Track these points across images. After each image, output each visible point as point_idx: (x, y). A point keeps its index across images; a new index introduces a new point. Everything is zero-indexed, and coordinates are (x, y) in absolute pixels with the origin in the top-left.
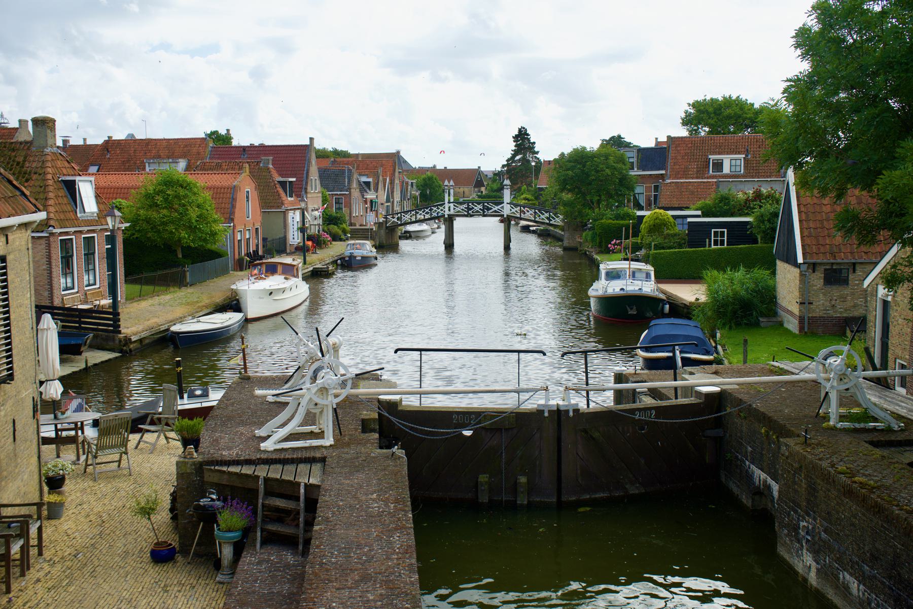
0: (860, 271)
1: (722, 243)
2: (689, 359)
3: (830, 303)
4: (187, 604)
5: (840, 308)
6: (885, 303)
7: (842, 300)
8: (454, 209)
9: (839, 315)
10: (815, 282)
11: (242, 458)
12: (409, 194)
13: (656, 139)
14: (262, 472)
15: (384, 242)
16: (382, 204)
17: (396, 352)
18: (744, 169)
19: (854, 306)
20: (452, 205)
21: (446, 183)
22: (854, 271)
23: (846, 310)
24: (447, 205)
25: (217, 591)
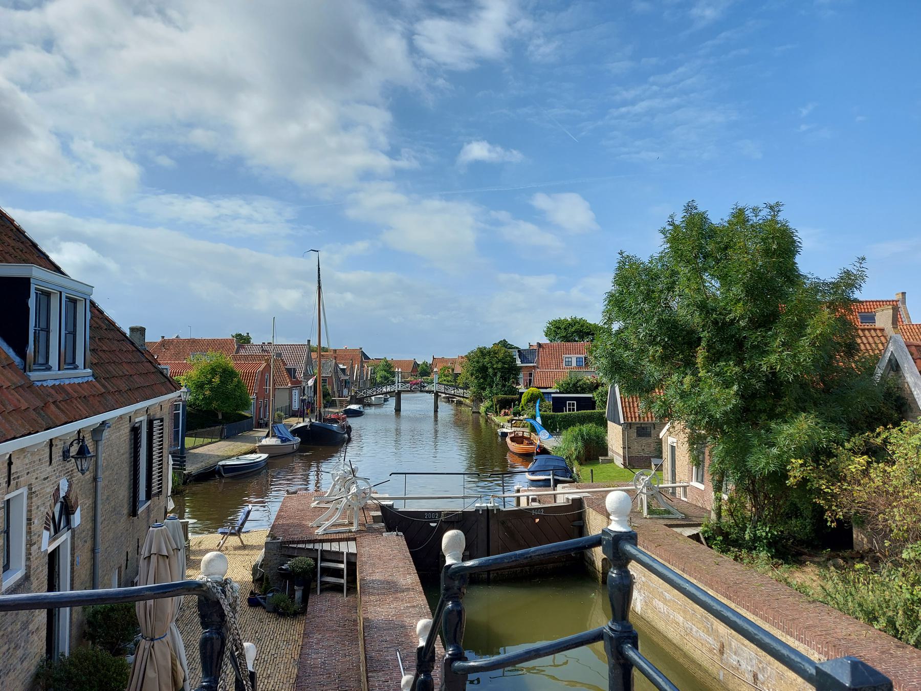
1: (573, 410)
2: (558, 480)
6: (673, 448)
17: (390, 475)
21: (396, 370)
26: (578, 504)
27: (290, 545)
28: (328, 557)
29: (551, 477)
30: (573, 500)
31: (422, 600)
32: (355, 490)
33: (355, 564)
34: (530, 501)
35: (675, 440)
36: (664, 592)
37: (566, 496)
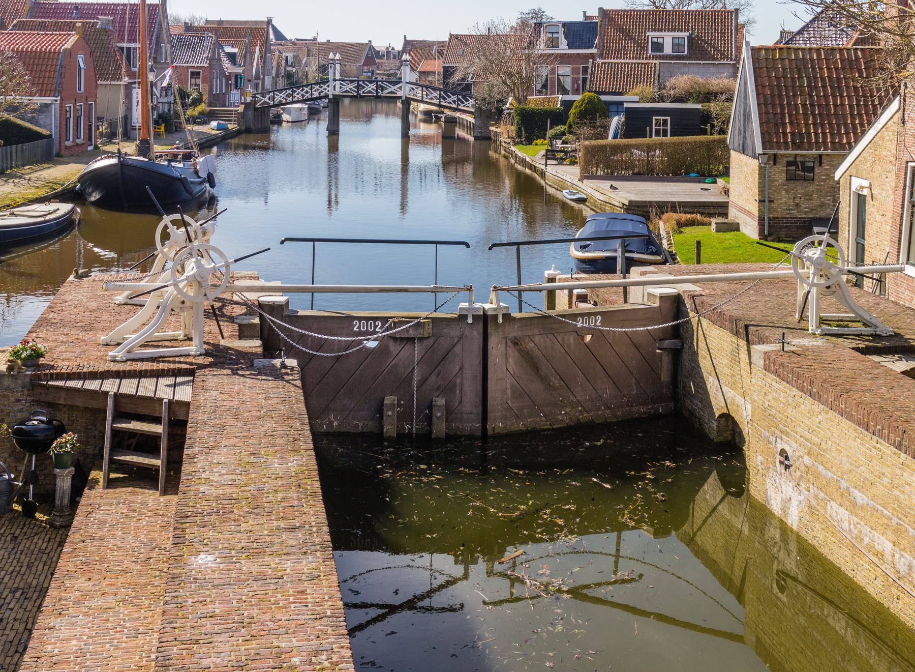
0: (828, 165)
3: (794, 201)
4: (9, 558)
5: (806, 208)
6: (861, 200)
7: (807, 198)
8: (341, 88)
9: (803, 216)
10: (776, 177)
11: (85, 370)
12: (283, 71)
13: (585, 13)
14: (110, 386)
15: (252, 127)
16: (249, 81)
18: (688, 49)
19: (822, 205)
20: (338, 82)
22: (820, 164)
23: (812, 210)
24: (331, 83)
25: (49, 541)
26: (675, 305)
27: (50, 383)
28: (130, 408)
29: (619, 254)
30: (662, 298)
31: (316, 514)
32: (195, 270)
33: (185, 423)
34: (574, 299)
35: (866, 183)
36: (851, 490)
37: (651, 289)
